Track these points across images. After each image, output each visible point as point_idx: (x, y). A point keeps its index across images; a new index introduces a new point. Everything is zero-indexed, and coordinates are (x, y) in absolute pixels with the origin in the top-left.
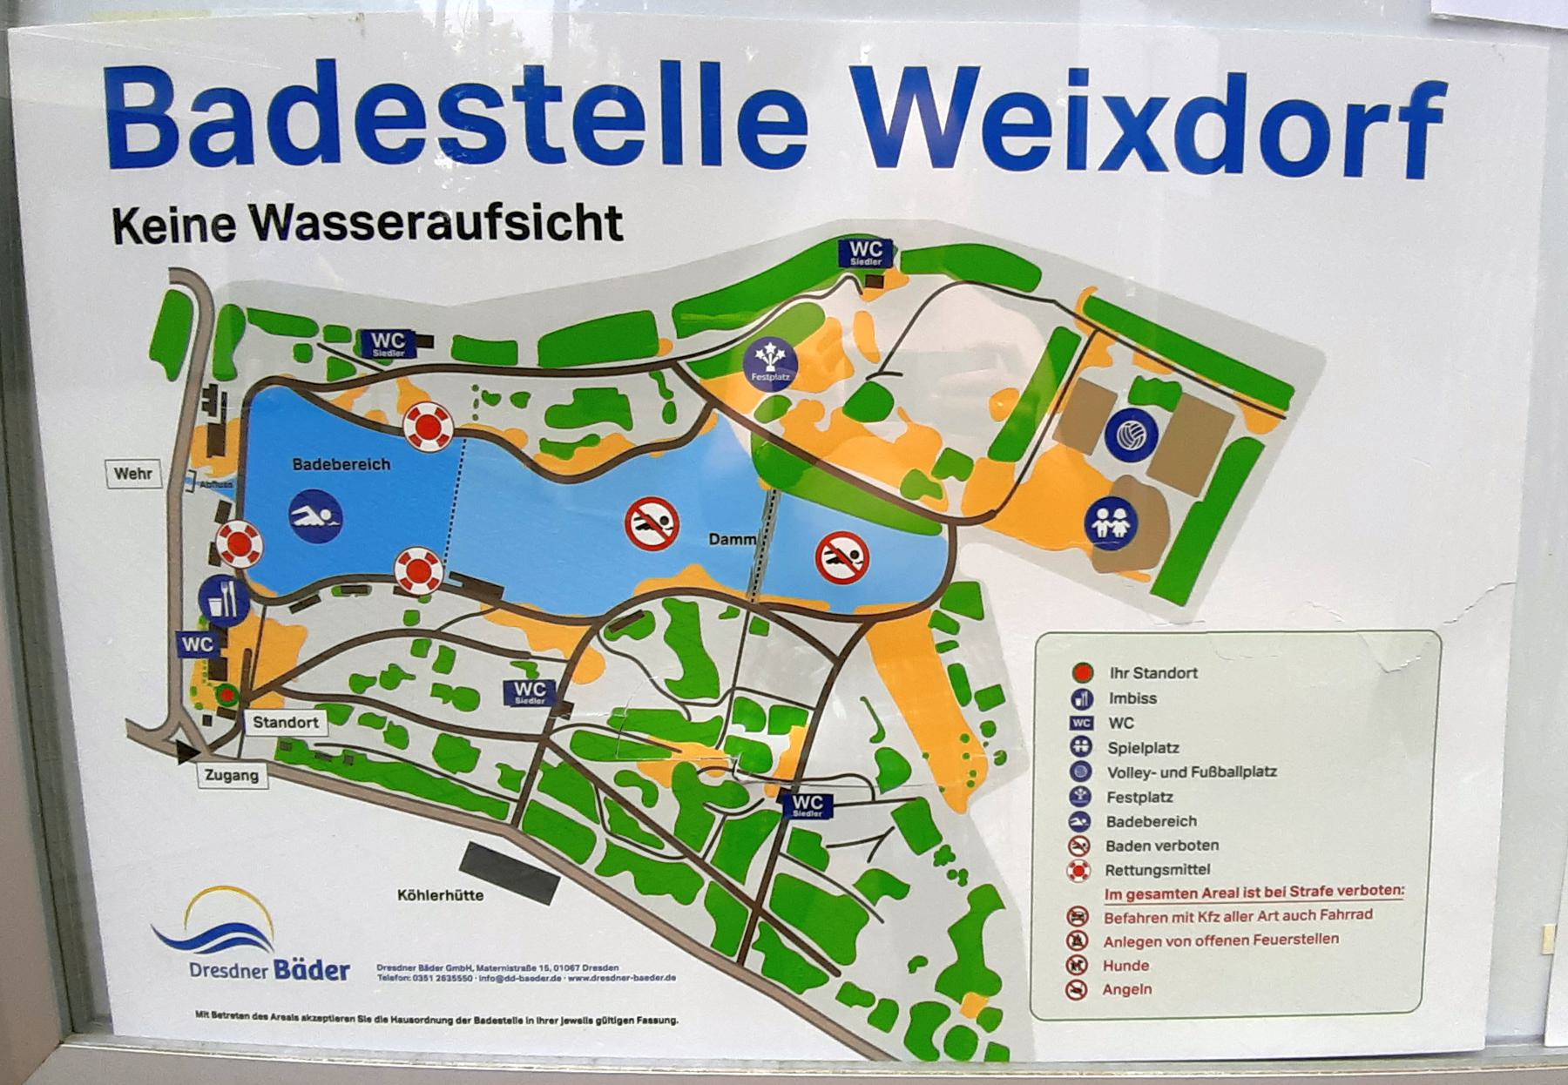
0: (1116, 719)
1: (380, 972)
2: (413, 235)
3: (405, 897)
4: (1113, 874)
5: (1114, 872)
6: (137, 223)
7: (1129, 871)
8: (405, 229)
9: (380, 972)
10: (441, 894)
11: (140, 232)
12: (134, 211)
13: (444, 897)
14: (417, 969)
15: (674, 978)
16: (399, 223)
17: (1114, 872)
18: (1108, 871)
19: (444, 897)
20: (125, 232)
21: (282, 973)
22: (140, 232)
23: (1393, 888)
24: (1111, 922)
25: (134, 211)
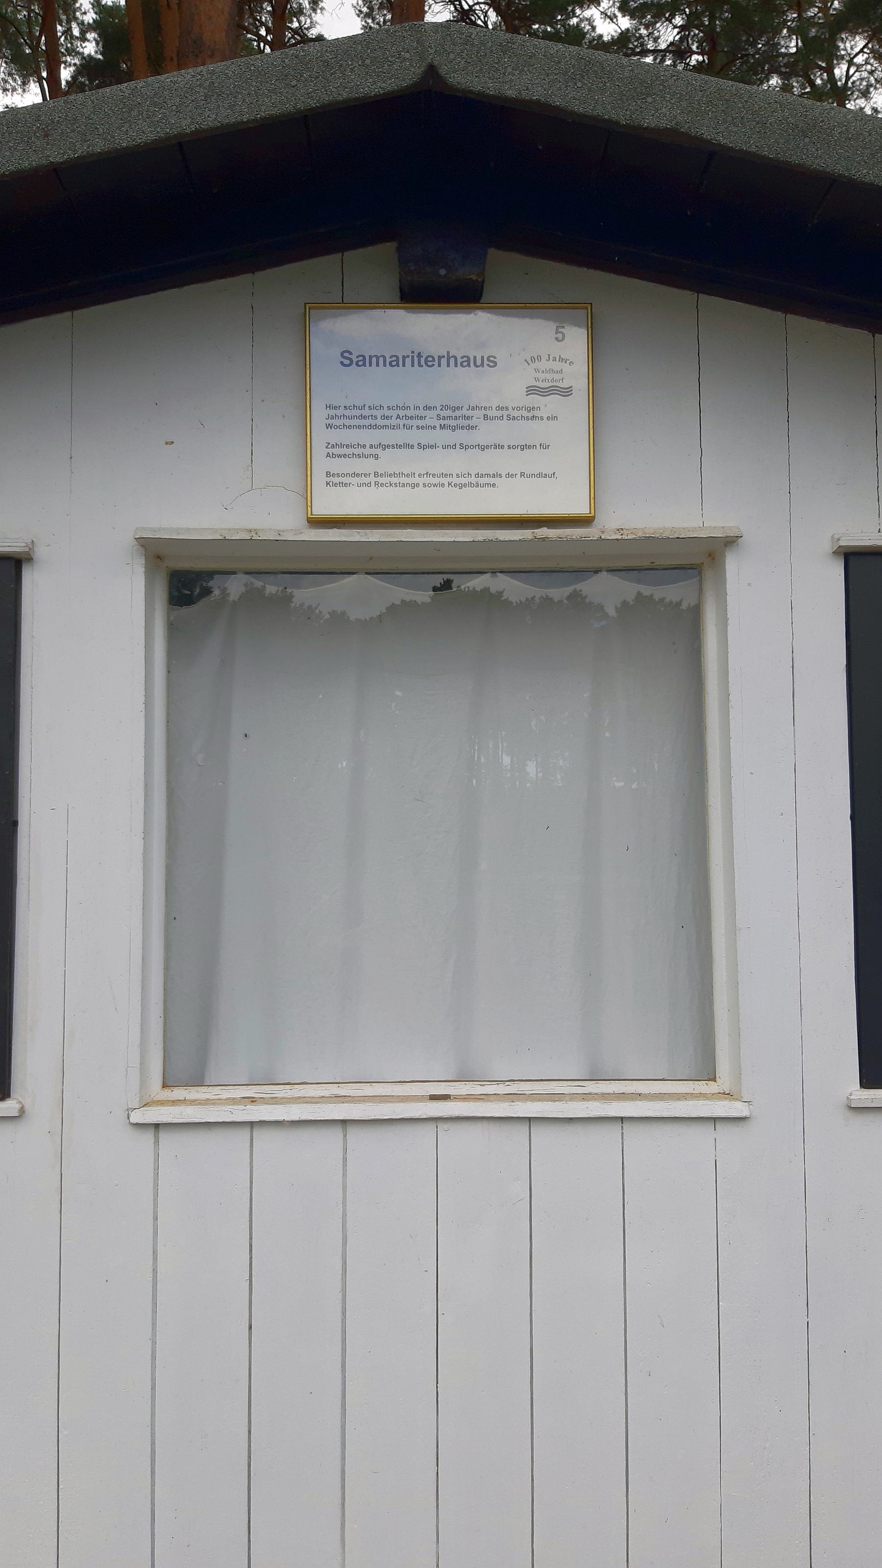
0: (435, 484)
1: (328, 479)
2: (439, 365)
3: (451, 485)
4: (524, 477)
5: (379, 485)
6: (453, 484)
7: (341, 485)
8: (436, 363)
9: (328, 479)
10: (440, 358)
11: (453, 486)
12: (452, 482)
13: (444, 361)
14: (372, 475)
15: (167, 443)
16: (434, 360)
17: (379, 485)
18: (521, 475)
19: (444, 361)
20: (450, 486)
21: (376, 476)
22: (453, 486)
23: (458, 484)
24: (330, 476)
25: (452, 482)
